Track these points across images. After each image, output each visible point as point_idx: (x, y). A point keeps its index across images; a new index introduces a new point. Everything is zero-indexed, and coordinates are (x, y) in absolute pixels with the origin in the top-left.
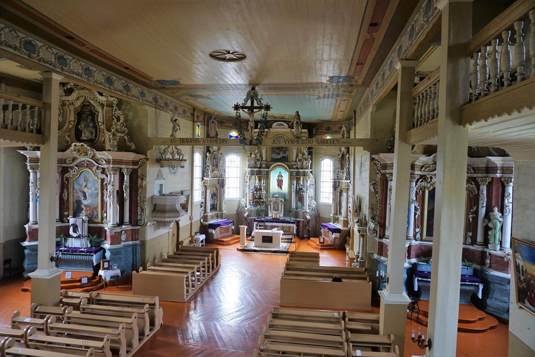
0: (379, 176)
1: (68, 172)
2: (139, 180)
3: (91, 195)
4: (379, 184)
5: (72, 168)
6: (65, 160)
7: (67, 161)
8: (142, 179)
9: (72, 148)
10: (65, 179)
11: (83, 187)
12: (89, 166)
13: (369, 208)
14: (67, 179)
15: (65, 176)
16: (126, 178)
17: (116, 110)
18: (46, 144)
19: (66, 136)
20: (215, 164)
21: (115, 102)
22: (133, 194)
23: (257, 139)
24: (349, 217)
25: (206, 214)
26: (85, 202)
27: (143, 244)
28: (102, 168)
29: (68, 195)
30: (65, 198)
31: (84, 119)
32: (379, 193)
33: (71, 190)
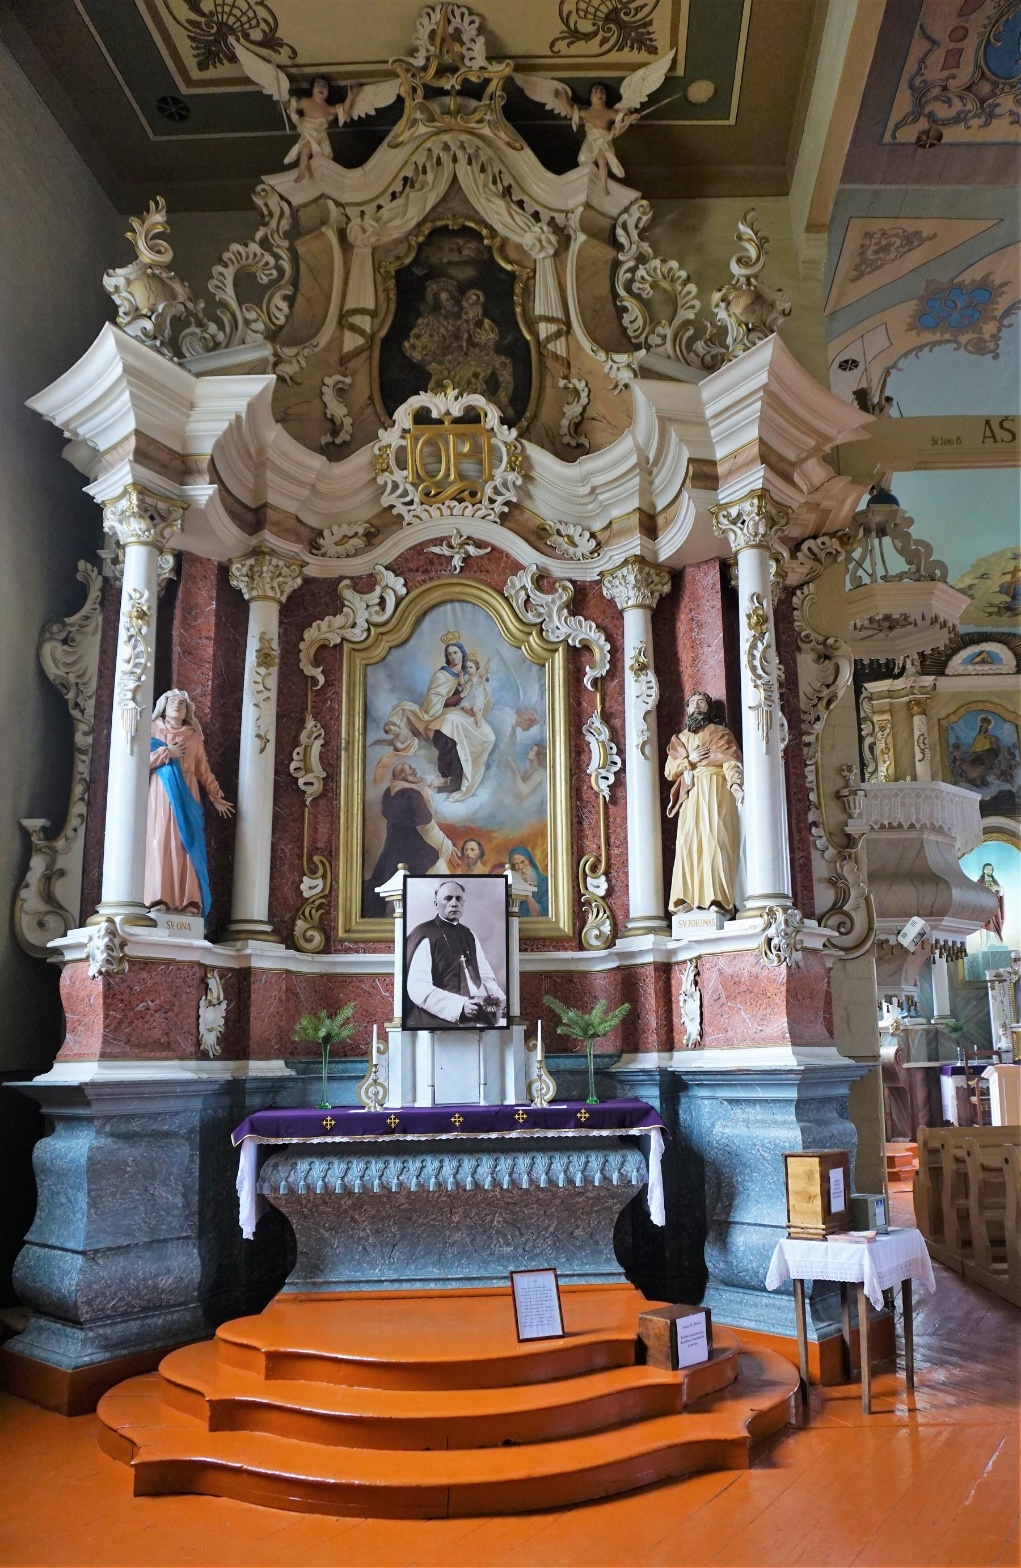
1: (337, 606)
3: (492, 759)
7: (327, 542)
10: (306, 650)
11: (438, 704)
12: (490, 567)
15: (311, 634)
26: (448, 807)
29: (330, 761)
30: (310, 781)
31: (437, 307)
33: (349, 725)
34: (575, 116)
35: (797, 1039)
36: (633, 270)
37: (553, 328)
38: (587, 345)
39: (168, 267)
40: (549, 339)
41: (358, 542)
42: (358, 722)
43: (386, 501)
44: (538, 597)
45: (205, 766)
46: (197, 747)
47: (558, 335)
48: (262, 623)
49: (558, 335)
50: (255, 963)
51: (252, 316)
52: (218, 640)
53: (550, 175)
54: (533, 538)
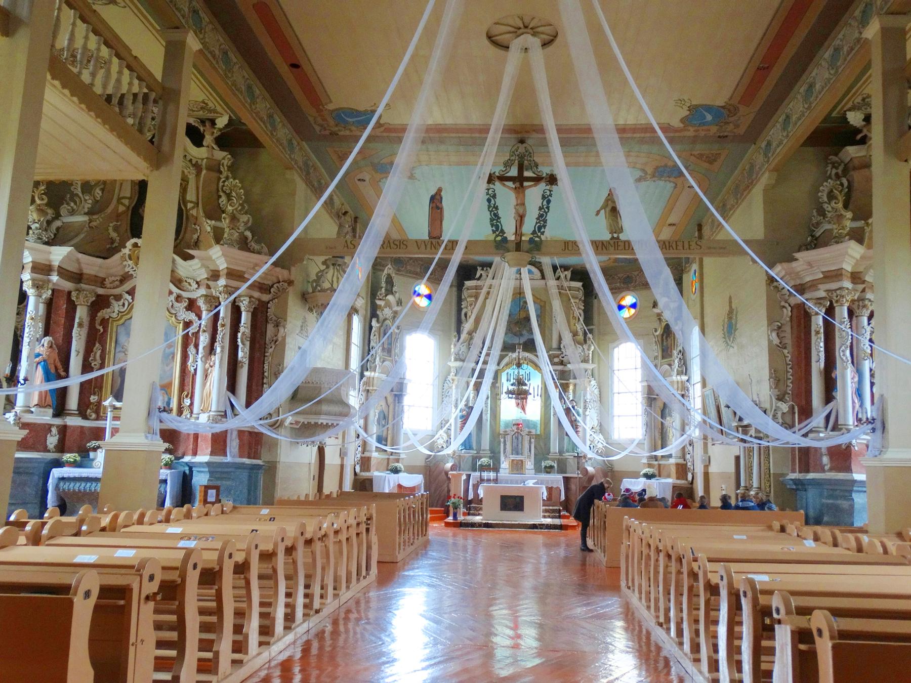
0: (787, 312)
2: (270, 328)
4: (788, 328)
5: (118, 298)
6: (104, 279)
7: (107, 282)
8: (277, 325)
9: (126, 251)
13: (771, 377)
14: (105, 322)
15: (99, 314)
16: (245, 318)
17: (227, 178)
18: (163, 168)
19: (111, 229)
20: (386, 346)
21: (225, 162)
22: (257, 355)
23: (531, 241)
24: (688, 456)
25: (367, 454)
27: (271, 469)
28: (189, 299)
32: (789, 347)
34: (202, 129)
35: (678, 478)
36: (224, 182)
37: (192, 205)
38: (201, 213)
39: (46, 205)
40: (191, 209)
41: (117, 283)
42: (113, 345)
43: (127, 270)
44: (176, 304)
45: (57, 360)
46: (55, 355)
47: (193, 208)
48: (81, 313)
49: (193, 208)
50: (68, 424)
51: (87, 198)
52: (66, 317)
53: (195, 148)
54: (177, 283)
